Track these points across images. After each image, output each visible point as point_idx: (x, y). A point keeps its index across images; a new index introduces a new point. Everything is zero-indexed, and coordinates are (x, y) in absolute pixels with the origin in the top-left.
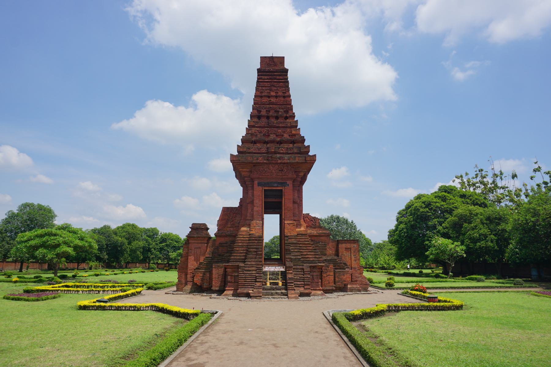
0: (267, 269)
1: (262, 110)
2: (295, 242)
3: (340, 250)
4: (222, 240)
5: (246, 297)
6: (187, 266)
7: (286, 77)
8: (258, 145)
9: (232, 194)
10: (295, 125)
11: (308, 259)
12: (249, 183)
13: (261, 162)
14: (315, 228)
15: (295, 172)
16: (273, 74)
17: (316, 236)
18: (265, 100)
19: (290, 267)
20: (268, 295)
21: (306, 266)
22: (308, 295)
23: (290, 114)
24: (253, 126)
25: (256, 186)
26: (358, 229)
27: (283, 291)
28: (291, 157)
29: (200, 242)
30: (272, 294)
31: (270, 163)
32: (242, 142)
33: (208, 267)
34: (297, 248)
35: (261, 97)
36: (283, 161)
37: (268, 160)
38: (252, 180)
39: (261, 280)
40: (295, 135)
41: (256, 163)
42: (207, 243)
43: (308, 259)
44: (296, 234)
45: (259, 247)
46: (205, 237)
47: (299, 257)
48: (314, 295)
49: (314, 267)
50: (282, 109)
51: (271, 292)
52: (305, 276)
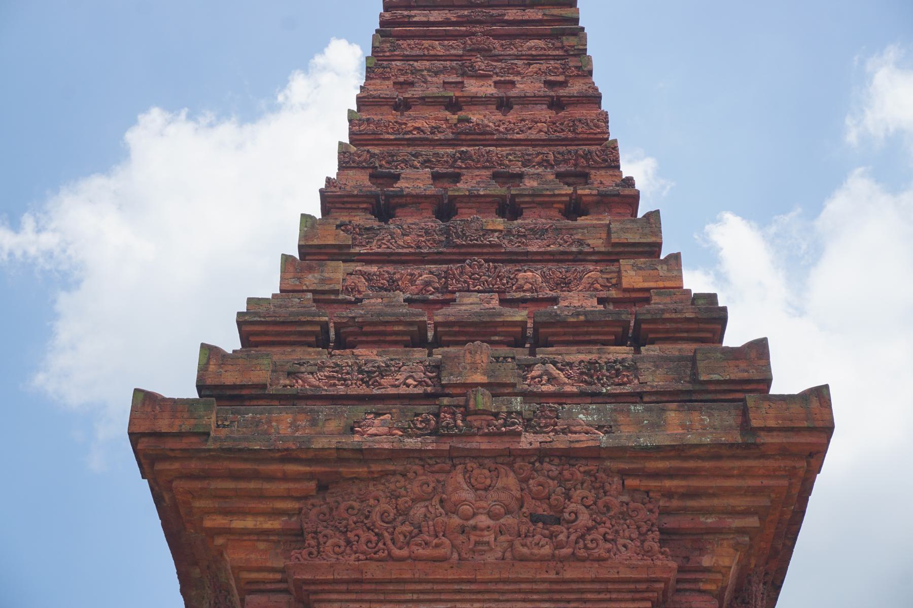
15: (667, 535)
24: (340, 253)
31: (453, 457)
36: (561, 442)
40: (642, 297)
41: (342, 456)
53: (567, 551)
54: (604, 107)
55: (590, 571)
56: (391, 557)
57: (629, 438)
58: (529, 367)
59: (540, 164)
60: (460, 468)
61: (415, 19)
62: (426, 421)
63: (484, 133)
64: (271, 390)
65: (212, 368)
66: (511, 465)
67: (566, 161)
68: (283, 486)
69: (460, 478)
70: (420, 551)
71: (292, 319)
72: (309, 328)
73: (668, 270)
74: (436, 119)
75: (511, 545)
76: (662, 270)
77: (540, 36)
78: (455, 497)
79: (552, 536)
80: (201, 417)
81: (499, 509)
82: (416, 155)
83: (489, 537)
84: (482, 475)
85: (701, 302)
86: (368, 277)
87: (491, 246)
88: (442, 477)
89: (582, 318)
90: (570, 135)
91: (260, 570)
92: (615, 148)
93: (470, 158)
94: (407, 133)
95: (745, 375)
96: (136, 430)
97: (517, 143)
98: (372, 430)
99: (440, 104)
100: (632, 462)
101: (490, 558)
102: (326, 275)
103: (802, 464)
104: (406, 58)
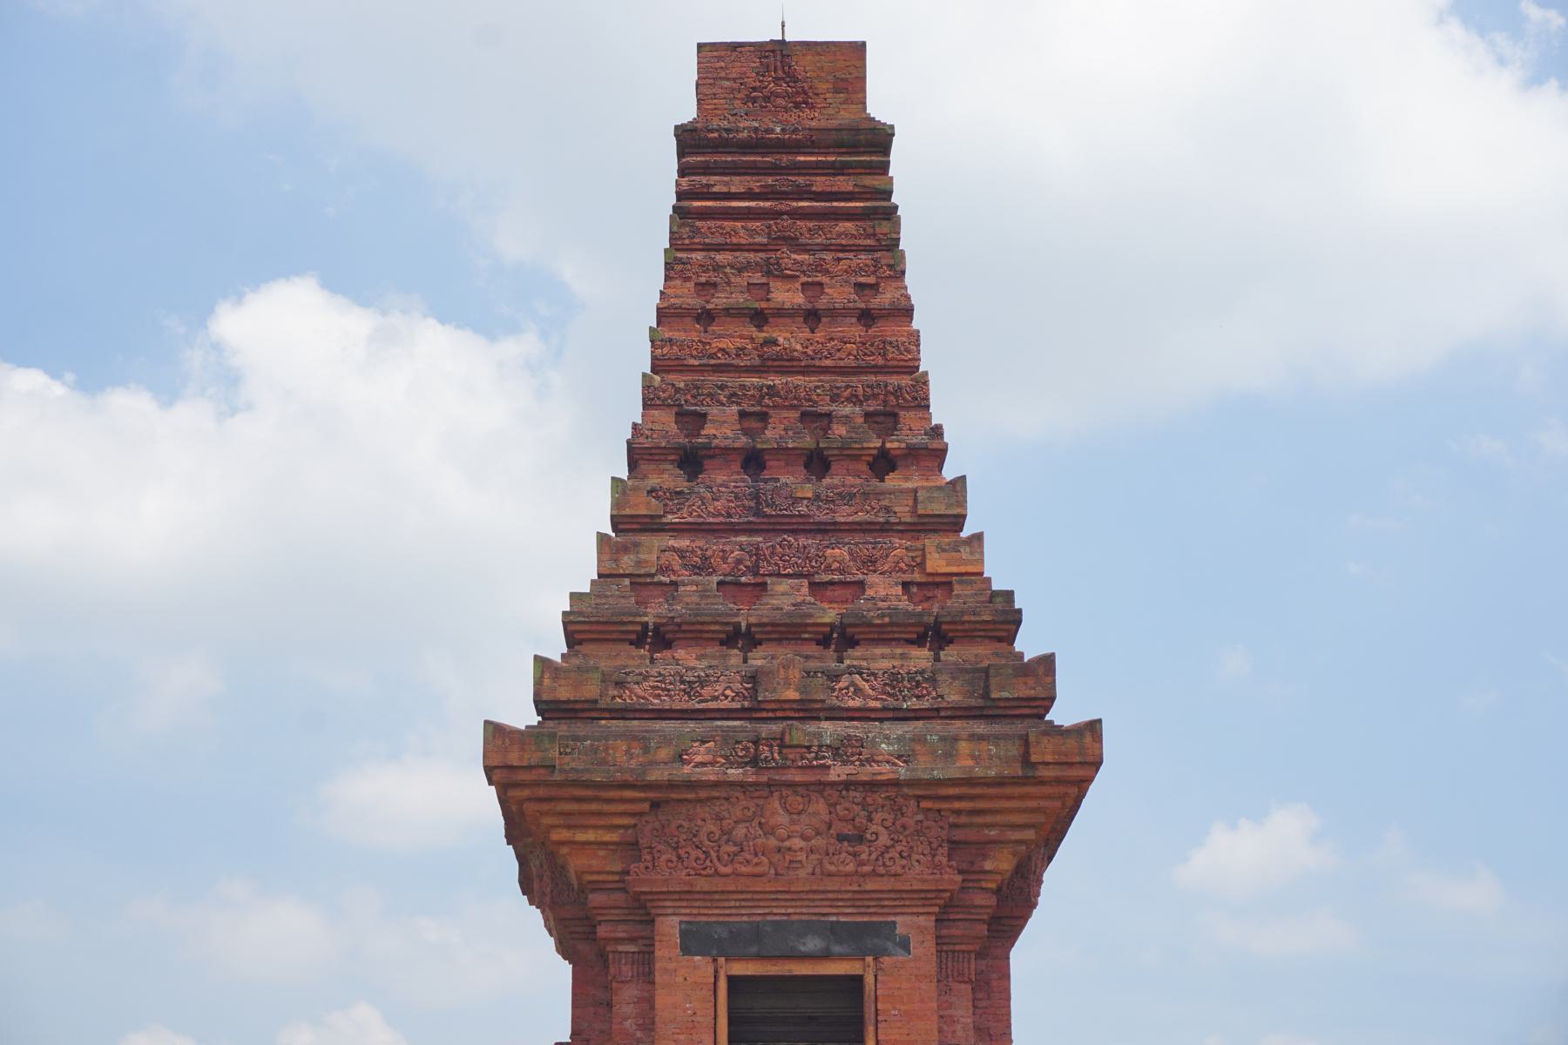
1: (714, 411)
8: (688, 658)
13: (709, 774)
16: (785, 164)
18: (732, 338)
24: (651, 525)
25: (667, 950)
28: (920, 739)
31: (770, 785)
35: (706, 317)
36: (867, 773)
37: (754, 761)
38: (643, 913)
40: (944, 583)
41: (672, 785)
50: (854, 399)
53: (867, 869)
54: (915, 325)
55: (888, 884)
56: (717, 873)
57: (924, 770)
58: (835, 677)
59: (848, 400)
60: (776, 795)
61: (715, 189)
62: (746, 749)
63: (792, 359)
64: (602, 705)
65: (546, 681)
66: (821, 792)
67: (875, 396)
68: (621, 808)
69: (777, 804)
70: (744, 869)
71: (615, 619)
72: (631, 628)
73: (972, 553)
74: (741, 337)
75: (821, 863)
76: (965, 553)
77: (850, 216)
78: (772, 822)
79: (855, 855)
80: (547, 750)
81: (810, 832)
82: (722, 388)
83: (801, 856)
84: (796, 801)
85: (999, 600)
86: (681, 553)
87: (800, 516)
88: (761, 802)
89: (887, 620)
90: (881, 362)
91: (599, 873)
92: (926, 383)
94: (711, 356)
95: (1032, 693)
96: (491, 763)
97: (826, 370)
98: (698, 759)
99: (745, 315)
100: (925, 790)
101: (802, 873)
102: (642, 556)
103: (1074, 791)
104: (708, 248)
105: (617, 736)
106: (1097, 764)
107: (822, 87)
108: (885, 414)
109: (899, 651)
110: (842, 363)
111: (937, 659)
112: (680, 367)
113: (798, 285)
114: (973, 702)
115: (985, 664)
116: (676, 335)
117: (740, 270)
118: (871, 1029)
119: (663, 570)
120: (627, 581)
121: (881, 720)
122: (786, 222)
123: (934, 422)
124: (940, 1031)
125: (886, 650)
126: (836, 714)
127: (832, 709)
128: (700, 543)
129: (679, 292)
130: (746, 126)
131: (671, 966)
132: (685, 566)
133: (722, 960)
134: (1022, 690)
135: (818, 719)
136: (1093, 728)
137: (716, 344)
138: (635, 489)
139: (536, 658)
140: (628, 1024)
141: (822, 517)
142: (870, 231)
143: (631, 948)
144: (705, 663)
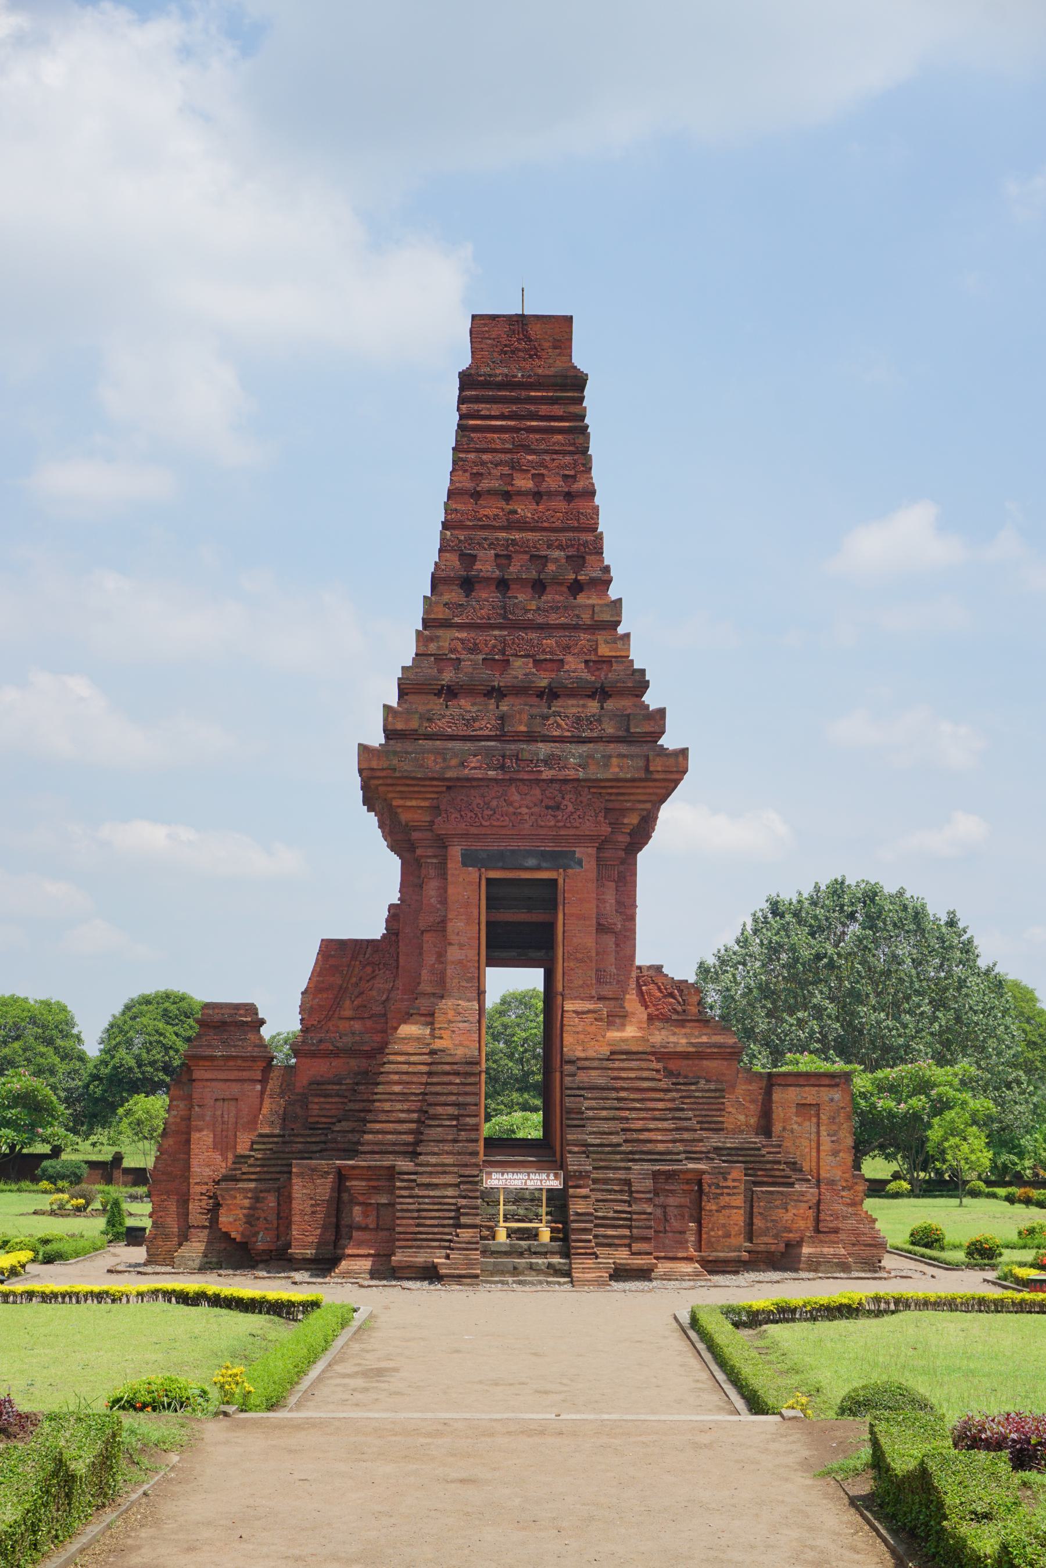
0: (495, 1180)
1: (481, 554)
2: (601, 1081)
3: (778, 1113)
4: (320, 1068)
5: (423, 1279)
6: (187, 1167)
7: (573, 409)
8: (466, 705)
9: (361, 886)
10: (608, 621)
11: (649, 1147)
12: (430, 852)
13: (478, 774)
14: (681, 1023)
15: (607, 810)
17: (685, 1056)
18: (492, 508)
19: (581, 1175)
20: (502, 1273)
21: (639, 1172)
22: (644, 1274)
23: (590, 572)
24: (446, 624)
25: (454, 863)
26: (982, 963)
27: (556, 1260)
28: (591, 757)
29: (234, 1075)
30: (515, 1271)
31: (511, 780)
32: (402, 693)
33: (274, 1170)
34: (609, 1103)
35: (476, 495)
37: (502, 767)
38: (442, 843)
39: (477, 1221)
40: (608, 661)
41: (458, 779)
42: (264, 1081)
43: (649, 1147)
44: (605, 1051)
45: (469, 1099)
46: (254, 1059)
47: (615, 1139)
48: (667, 1277)
49: (670, 1175)
50: (561, 547)
51: (515, 1262)
52: (635, 1208)
55: (572, 832)
56: (481, 825)
59: (557, 548)
62: (498, 760)
64: (420, 732)
65: (390, 719)
67: (572, 546)
68: (431, 789)
69: (514, 790)
70: (495, 823)
74: (497, 508)
76: (620, 644)
79: (554, 816)
81: (531, 805)
83: (527, 817)
86: (462, 641)
92: (601, 539)
93: (517, 544)
94: (480, 520)
95: (652, 729)
97: (545, 529)
98: (472, 765)
100: (594, 784)
101: (527, 826)
105: (430, 751)
106: (685, 772)
107: (546, 345)
108: (577, 557)
109: (581, 702)
110: (554, 525)
111: (602, 708)
112: (461, 526)
113: (530, 476)
114: (620, 733)
115: (629, 711)
116: (459, 507)
117: (496, 465)
118: (561, 907)
119: (451, 651)
120: (432, 659)
121: (570, 742)
122: (524, 435)
123: (606, 563)
124: (598, 906)
125: (574, 702)
126: (547, 739)
127: (544, 736)
128: (473, 635)
129: (461, 479)
130: (501, 372)
131: (457, 872)
132: (464, 649)
133: (483, 870)
134: (647, 728)
135: (537, 741)
136: (684, 752)
137: (483, 512)
138: (437, 603)
139: (385, 706)
140: (432, 900)
141: (540, 620)
142: (572, 441)
143: (435, 861)
144: (475, 708)
